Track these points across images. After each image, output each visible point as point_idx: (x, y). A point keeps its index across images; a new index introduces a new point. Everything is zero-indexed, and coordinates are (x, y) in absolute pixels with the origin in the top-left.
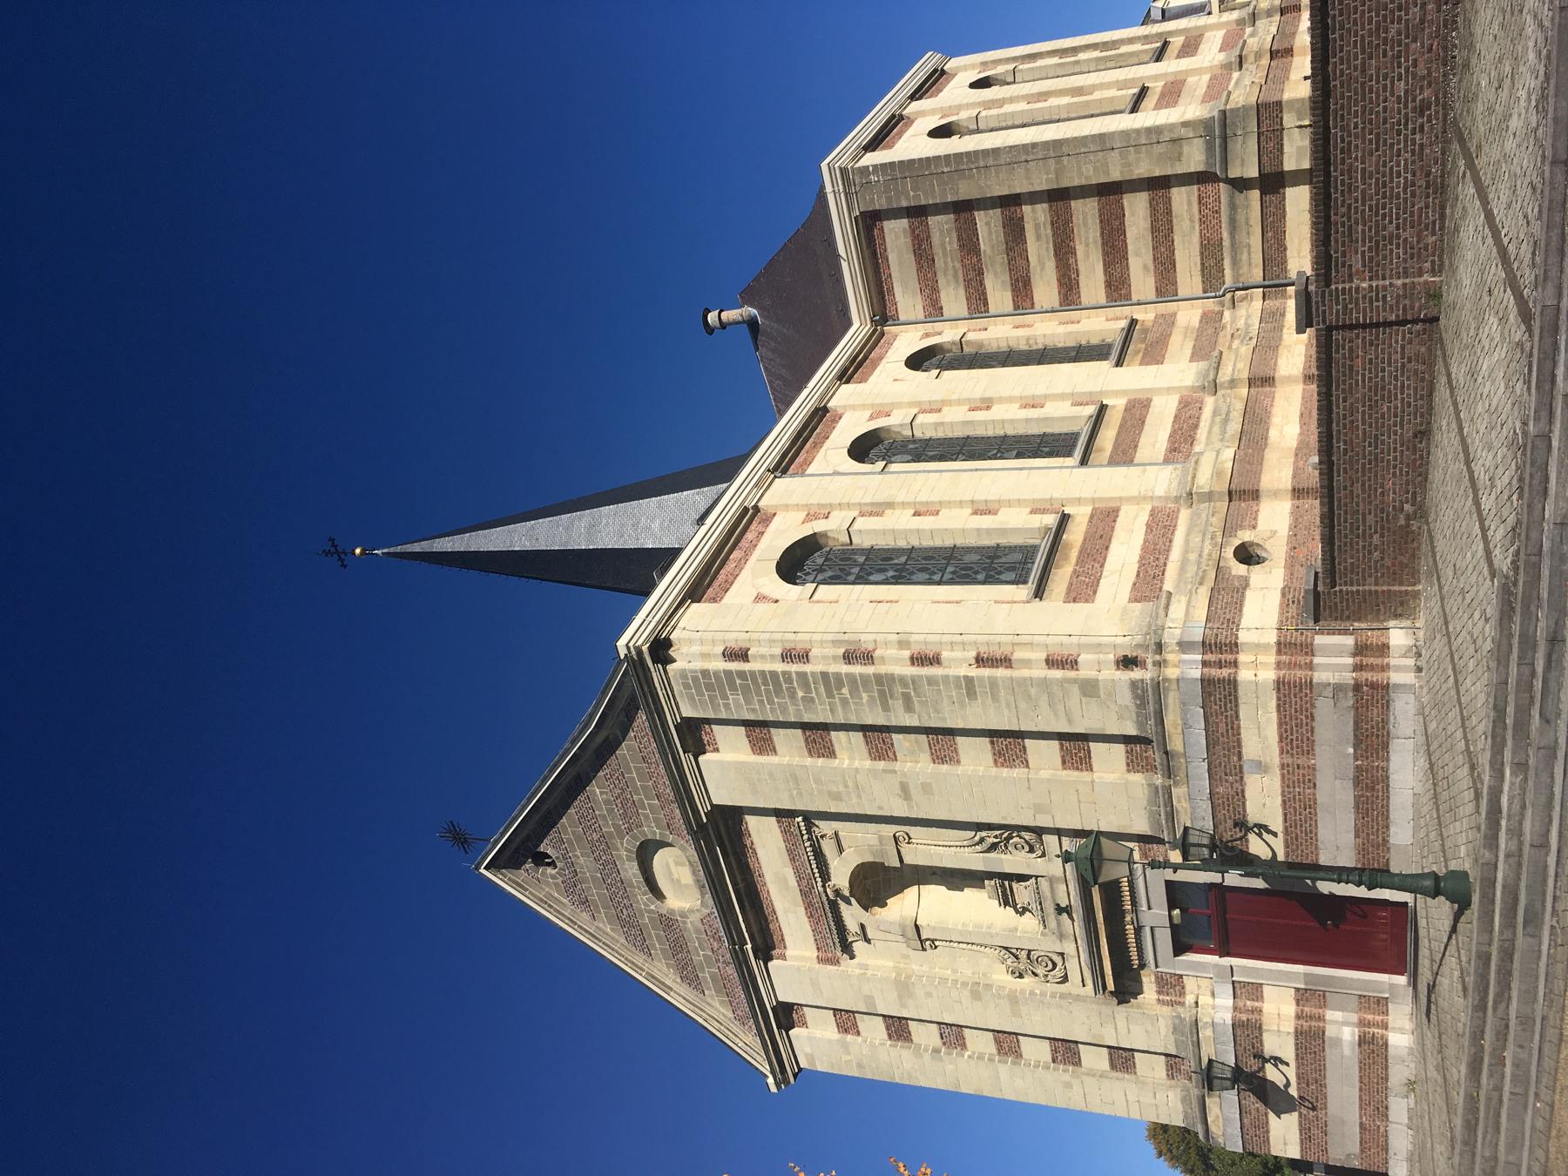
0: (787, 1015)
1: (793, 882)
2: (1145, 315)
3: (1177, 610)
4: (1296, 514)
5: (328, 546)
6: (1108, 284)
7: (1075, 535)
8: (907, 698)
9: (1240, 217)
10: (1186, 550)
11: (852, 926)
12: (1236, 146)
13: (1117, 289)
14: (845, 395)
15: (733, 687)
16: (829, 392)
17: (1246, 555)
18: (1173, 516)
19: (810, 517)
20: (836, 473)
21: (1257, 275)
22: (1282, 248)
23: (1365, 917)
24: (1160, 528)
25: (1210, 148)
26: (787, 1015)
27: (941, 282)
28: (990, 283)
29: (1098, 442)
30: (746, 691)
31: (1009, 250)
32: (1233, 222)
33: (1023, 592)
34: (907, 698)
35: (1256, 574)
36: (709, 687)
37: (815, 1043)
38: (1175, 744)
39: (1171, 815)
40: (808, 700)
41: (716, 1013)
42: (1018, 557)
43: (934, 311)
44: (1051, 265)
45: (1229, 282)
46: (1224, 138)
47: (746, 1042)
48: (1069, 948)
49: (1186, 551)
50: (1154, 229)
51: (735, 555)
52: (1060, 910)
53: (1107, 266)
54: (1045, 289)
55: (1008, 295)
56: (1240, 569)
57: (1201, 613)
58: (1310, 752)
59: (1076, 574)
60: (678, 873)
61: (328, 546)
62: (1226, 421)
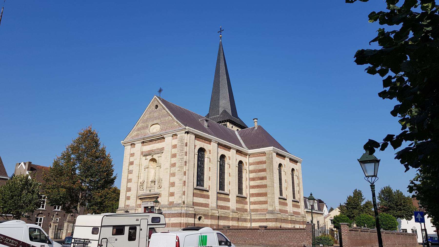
0: (133, 145)
1: (154, 149)
2: (248, 200)
3: (191, 209)
4: (192, 224)
5: (222, 29)
6: (253, 194)
7: (205, 193)
8: (180, 170)
9: (261, 215)
10: (201, 209)
11: (148, 157)
12: (271, 215)
13: (252, 195)
14: (233, 152)
15: (181, 144)
16: (233, 148)
17: (200, 218)
18: (208, 207)
19: (210, 151)
20: (218, 153)
21: (252, 218)
22: (256, 222)
23: (180, 180)
24: (206, 205)
25: (271, 211)
26: (133, 145)
27: (255, 166)
28: (254, 174)
29: (222, 195)
30: (181, 146)
31: (259, 177)
32: (260, 214)
33: (195, 186)
34: (180, 170)
35: (197, 220)
36: (182, 140)
37: (128, 149)
38: (173, 209)
39: (163, 208)
40: (180, 155)
41: (133, 133)
42: (202, 184)
43: (250, 164)
44: (256, 184)
45: (252, 213)
46: (272, 213)
47: (128, 138)
48: (145, 191)
49: (199, 209)
50: (260, 201)
51: (203, 141)
52: (150, 191)
53: (255, 194)
54: (253, 183)
55: (252, 177)
56: (198, 217)
57: (190, 212)
58: (171, 227)
59: (198, 194)
60: (155, 129)
61: (222, 29)
62: (224, 214)
